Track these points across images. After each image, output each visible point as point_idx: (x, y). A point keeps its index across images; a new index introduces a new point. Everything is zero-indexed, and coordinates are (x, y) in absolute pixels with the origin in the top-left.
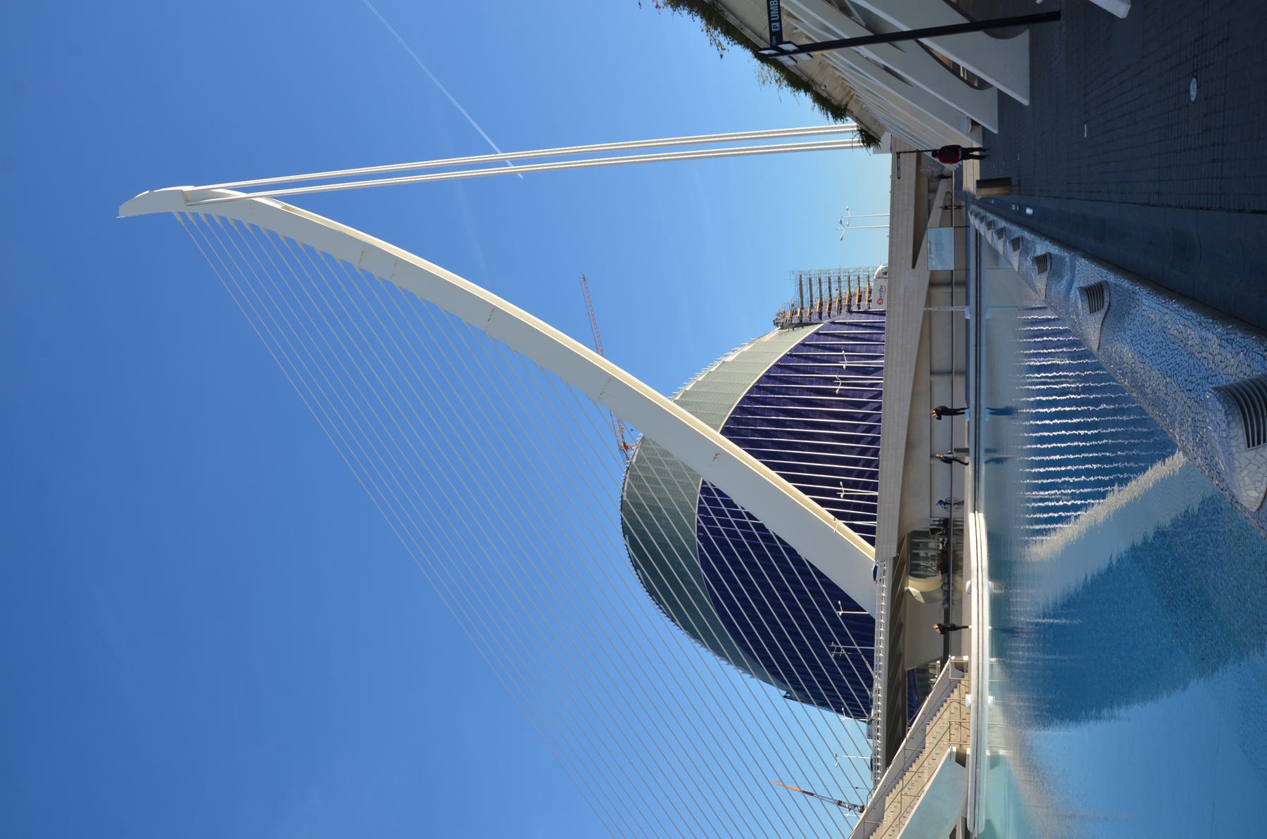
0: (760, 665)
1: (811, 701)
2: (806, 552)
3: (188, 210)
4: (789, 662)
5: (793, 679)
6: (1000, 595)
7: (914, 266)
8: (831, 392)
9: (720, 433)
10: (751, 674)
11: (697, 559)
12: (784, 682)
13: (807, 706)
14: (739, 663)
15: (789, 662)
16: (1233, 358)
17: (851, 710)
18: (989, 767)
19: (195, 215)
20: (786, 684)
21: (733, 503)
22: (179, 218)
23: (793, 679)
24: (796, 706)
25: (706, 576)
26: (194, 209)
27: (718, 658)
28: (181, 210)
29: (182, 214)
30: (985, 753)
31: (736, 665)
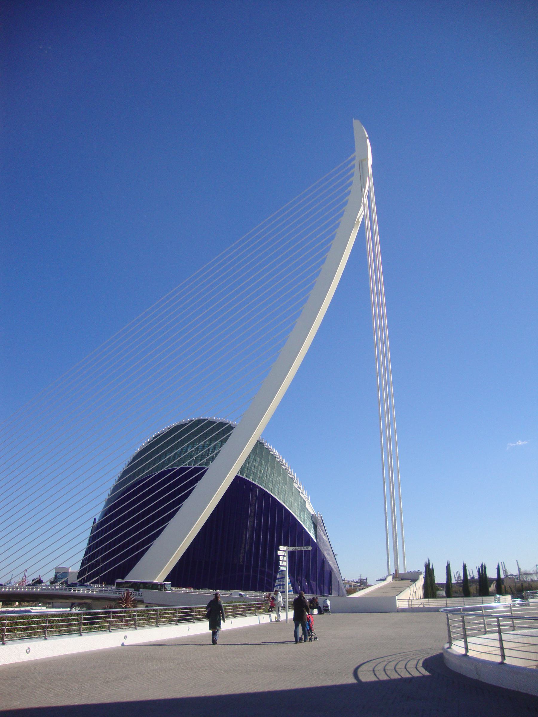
0: (115, 501)
1: (83, 567)
2: (172, 524)
3: (356, 162)
4: (110, 523)
5: (95, 546)
6: (429, 675)
7: (472, 570)
8: (85, 619)
9: (236, 475)
10: (111, 494)
11: (167, 468)
12: (102, 518)
13: (87, 541)
14: (116, 488)
15: (110, 523)
16: (151, 697)
17: (86, 558)
18: (234, 435)
19: (353, 166)
20: (102, 519)
21: (185, 499)
22: (352, 156)
23: (95, 546)
24: (90, 524)
25: (156, 474)
26: (357, 166)
27: (112, 488)
28: (356, 158)
29: (354, 159)
30: (306, 614)
31: (115, 486)
